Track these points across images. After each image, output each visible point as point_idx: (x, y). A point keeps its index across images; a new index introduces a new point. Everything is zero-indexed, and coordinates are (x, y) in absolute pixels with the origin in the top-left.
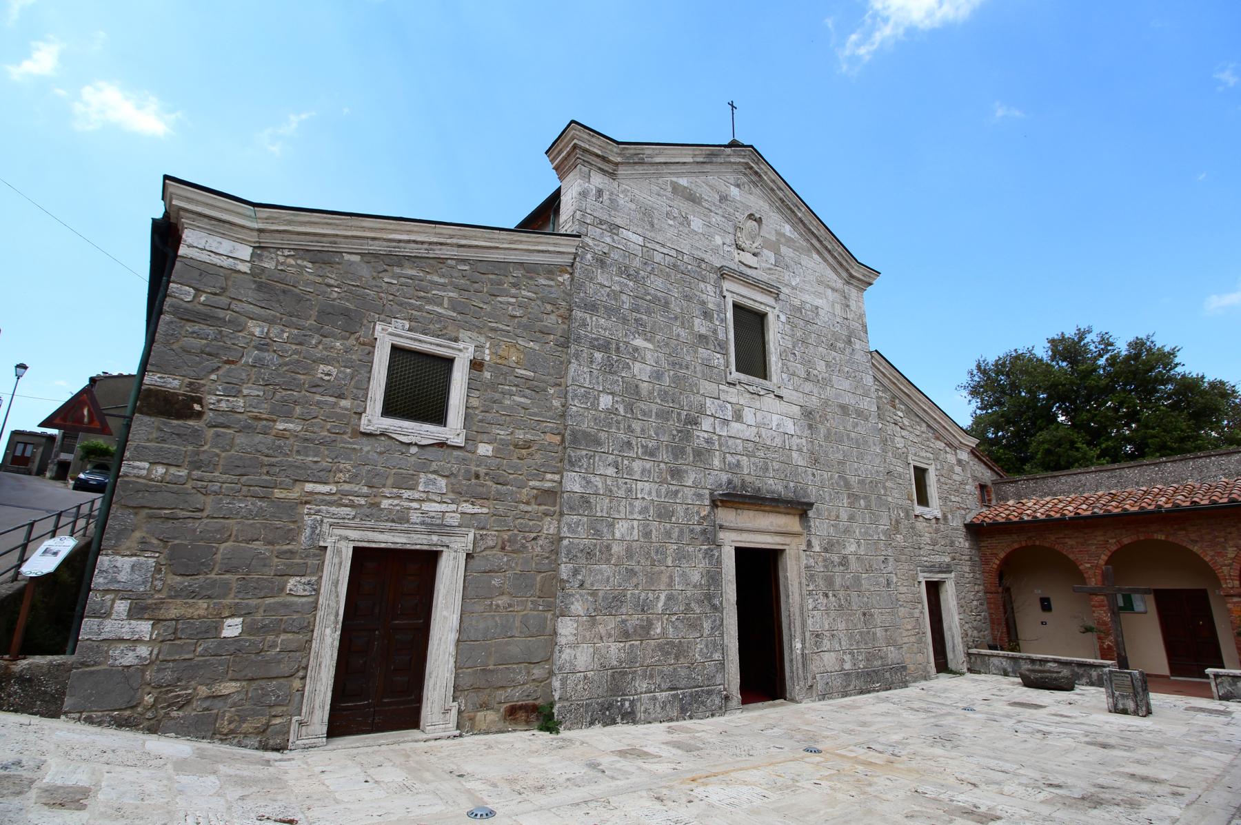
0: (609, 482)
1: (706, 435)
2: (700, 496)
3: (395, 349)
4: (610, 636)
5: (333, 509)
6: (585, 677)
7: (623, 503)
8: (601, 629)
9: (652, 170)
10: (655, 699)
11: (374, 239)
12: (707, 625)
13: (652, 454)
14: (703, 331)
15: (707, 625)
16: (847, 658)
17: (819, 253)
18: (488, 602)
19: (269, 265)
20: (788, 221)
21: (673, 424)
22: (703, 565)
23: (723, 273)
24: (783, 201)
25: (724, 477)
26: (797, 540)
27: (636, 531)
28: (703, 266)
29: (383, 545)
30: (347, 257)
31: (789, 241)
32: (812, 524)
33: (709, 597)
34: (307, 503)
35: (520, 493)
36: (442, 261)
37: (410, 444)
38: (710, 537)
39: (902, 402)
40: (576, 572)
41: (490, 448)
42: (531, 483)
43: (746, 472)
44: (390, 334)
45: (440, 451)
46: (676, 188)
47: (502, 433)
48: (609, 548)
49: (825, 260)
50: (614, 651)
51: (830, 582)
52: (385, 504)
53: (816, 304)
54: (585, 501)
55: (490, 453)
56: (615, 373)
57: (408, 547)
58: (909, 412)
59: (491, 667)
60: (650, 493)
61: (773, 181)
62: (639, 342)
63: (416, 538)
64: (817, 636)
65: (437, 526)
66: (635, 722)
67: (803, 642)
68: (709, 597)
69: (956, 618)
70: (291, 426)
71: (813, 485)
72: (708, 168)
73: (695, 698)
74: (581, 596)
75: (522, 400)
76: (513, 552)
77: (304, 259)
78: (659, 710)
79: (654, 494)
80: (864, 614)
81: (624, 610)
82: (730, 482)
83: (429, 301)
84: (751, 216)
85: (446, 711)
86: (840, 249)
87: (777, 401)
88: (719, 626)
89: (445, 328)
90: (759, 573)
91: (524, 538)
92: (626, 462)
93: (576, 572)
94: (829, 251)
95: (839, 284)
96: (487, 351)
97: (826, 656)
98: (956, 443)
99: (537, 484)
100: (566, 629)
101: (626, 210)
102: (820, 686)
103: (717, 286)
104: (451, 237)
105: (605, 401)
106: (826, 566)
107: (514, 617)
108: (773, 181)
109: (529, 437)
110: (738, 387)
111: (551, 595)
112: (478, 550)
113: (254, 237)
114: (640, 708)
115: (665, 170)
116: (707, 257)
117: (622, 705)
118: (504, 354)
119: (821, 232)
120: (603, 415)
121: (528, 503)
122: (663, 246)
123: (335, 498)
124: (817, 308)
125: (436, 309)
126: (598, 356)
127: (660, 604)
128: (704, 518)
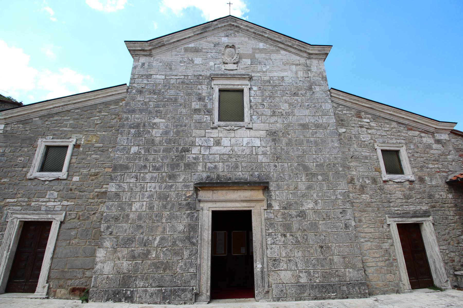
0: (131, 185)
1: (194, 156)
2: (187, 186)
4: (124, 258)
5: (14, 208)
6: (108, 277)
7: (138, 194)
8: (120, 255)
9: (172, 46)
10: (146, 291)
11: (41, 110)
12: (186, 254)
13: (158, 169)
14: (197, 107)
15: (186, 254)
16: (303, 275)
17: (284, 49)
18: (68, 242)
19: (9, 129)
20: (261, 41)
21: (173, 154)
22: (186, 221)
23: (212, 78)
24: (255, 33)
25: (205, 175)
26: (260, 204)
27: (144, 207)
28: (201, 78)
29: (30, 220)
30: (34, 119)
31: (261, 51)
32: (273, 193)
33: (189, 238)
34: (6, 206)
35: (89, 195)
36: (69, 111)
37: (45, 181)
38: (192, 207)
39: (366, 113)
40: (108, 228)
41: (78, 178)
42: (95, 190)
43: (220, 170)
44: (45, 142)
45: (56, 182)
46: (186, 50)
47: (85, 171)
48: (128, 216)
49: (290, 52)
50: (125, 265)
51: (288, 227)
52: (33, 204)
53: (282, 75)
54: (117, 195)
55: (78, 180)
56: (141, 136)
57: (39, 220)
58: (375, 118)
59: (66, 270)
60: (155, 188)
61: (247, 26)
62: (157, 120)
63: (42, 216)
65: (49, 211)
66: (132, 302)
67: (263, 264)
68: (189, 238)
69: (437, 249)
70: (6, 180)
71: (273, 173)
72: (206, 34)
73: (173, 292)
74: (110, 238)
75: (96, 156)
76: (83, 220)
77: (19, 124)
78: (148, 297)
79: (157, 188)
80: (322, 247)
81: (133, 245)
82: (208, 177)
83: (63, 127)
84: (227, 46)
85: (44, 287)
86: (297, 43)
87: (248, 131)
88: (195, 254)
89: (66, 135)
91: (89, 214)
92: (142, 175)
93: (108, 228)
94: (291, 46)
95: (303, 61)
96: (83, 140)
97: (282, 274)
98: (432, 130)
99: (98, 190)
100: (101, 254)
101: (157, 67)
102: (275, 292)
103: (209, 84)
104: (69, 101)
105: (134, 149)
107: (79, 248)
108: (247, 26)
109: (97, 171)
110: (219, 129)
111: (97, 239)
112: (67, 220)
114: (136, 295)
115: (179, 43)
116: (202, 74)
117: (126, 293)
118: (90, 139)
119: (283, 39)
120: (132, 156)
121: (93, 199)
122: (176, 76)
123: (15, 203)
124: (283, 77)
125: (65, 129)
126: (133, 131)
127: (156, 242)
128: (189, 197)
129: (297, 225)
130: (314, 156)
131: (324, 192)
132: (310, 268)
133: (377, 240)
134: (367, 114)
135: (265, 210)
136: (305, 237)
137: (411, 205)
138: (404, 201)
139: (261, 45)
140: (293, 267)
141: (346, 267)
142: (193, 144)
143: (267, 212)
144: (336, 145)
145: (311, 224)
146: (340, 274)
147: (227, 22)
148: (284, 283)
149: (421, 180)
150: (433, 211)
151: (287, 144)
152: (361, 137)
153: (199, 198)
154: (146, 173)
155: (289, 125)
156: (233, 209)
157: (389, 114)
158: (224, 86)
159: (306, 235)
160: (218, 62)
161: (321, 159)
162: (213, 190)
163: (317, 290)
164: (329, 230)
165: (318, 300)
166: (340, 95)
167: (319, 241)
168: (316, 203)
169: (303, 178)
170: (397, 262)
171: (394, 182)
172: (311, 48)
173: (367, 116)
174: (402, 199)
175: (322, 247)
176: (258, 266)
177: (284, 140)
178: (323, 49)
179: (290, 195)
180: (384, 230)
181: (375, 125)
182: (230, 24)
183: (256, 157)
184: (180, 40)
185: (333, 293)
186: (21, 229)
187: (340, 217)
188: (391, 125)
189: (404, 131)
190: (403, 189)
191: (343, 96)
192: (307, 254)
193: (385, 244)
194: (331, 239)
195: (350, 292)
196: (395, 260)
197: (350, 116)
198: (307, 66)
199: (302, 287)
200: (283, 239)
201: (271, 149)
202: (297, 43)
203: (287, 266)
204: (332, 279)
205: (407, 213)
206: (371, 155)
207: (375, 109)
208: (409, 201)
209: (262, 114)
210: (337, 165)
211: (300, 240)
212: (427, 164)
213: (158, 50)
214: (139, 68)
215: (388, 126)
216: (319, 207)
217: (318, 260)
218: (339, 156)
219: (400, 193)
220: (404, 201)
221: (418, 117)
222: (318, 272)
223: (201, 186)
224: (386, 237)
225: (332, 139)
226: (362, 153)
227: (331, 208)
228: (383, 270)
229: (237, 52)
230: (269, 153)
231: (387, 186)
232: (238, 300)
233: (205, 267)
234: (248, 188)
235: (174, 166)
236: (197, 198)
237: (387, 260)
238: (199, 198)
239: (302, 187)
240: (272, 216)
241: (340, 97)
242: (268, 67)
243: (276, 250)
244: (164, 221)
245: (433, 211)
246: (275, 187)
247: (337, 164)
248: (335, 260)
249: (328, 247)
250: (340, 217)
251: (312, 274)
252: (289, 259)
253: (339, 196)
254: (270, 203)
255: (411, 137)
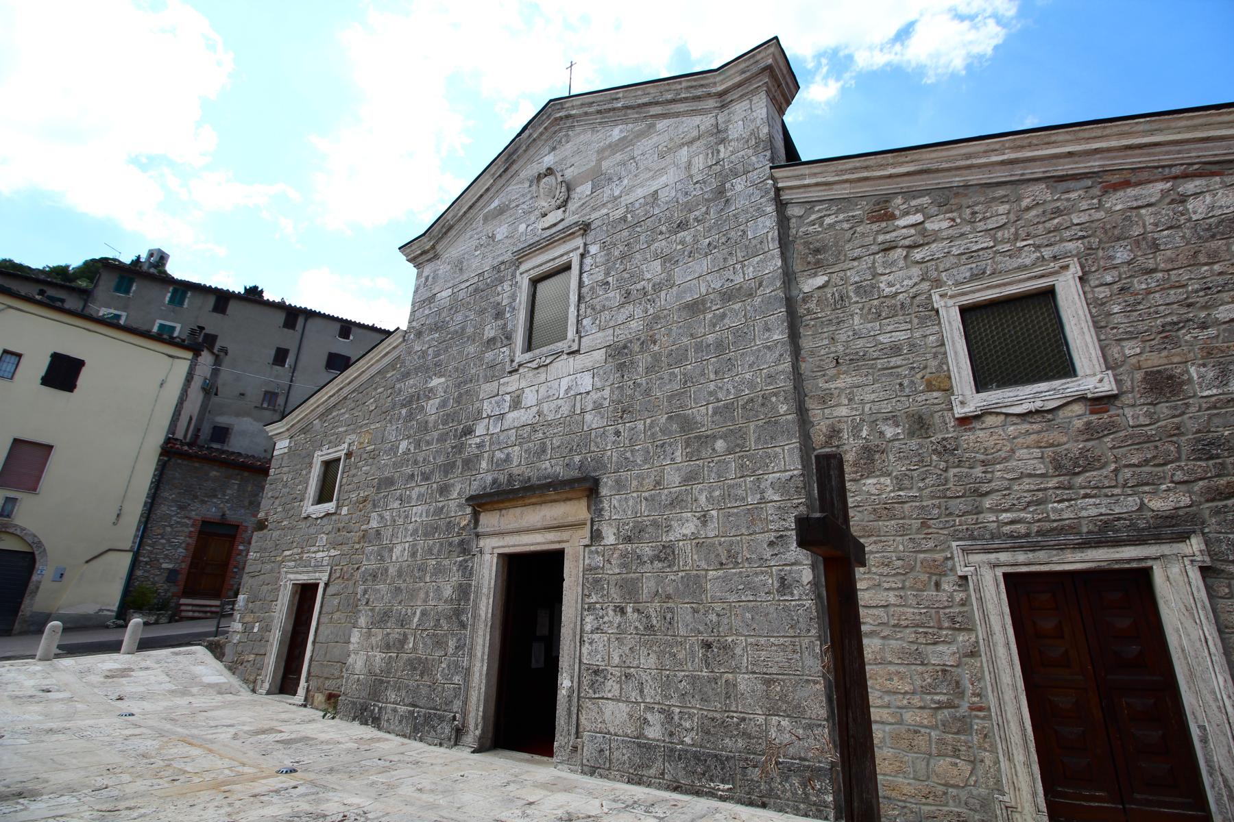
3: (965, 311)
10: (395, 710)
12: (452, 643)
15: (452, 643)
17: (664, 116)
20: (615, 123)
22: (456, 578)
31: (614, 148)
32: (606, 505)
33: (458, 613)
39: (910, 194)
48: (387, 570)
49: (677, 115)
51: (630, 589)
58: (946, 199)
64: (596, 672)
66: (379, 728)
68: (458, 613)
72: (515, 167)
73: (428, 719)
80: (708, 646)
82: (495, 481)
90: (533, 584)
93: (365, 592)
102: (588, 751)
106: (624, 565)
113: (287, 434)
127: (416, 620)
129: (652, 584)
130: (712, 386)
131: (730, 486)
132: (673, 702)
133: (909, 634)
134: (914, 198)
135: (586, 546)
136: (669, 616)
137: (1086, 496)
138: (1052, 483)
139: (616, 133)
140: (634, 694)
141: (772, 711)
142: (478, 416)
143: (591, 552)
144: (776, 337)
145: (687, 580)
146: (753, 730)
147: (548, 117)
148: (609, 733)
149: (1162, 385)
150: (1217, 512)
151: (649, 370)
152: (882, 285)
153: (480, 530)
154: (413, 488)
155: (657, 318)
156: (532, 548)
157: (1003, 163)
158: (551, 263)
159: (670, 610)
160: (533, 219)
161: (727, 390)
162: (500, 510)
163: (681, 765)
164: (733, 598)
165: (681, 793)
166: (802, 177)
167: (701, 629)
168: (704, 519)
169: (678, 453)
170: (989, 717)
171: (1007, 415)
172: (718, 79)
173: (913, 203)
174: (1042, 475)
175: (708, 646)
176: (565, 683)
177: (643, 360)
178: (752, 61)
179: (644, 503)
180: (943, 597)
181: (946, 224)
182: (556, 119)
183: (580, 418)
184: (474, 204)
185: (723, 782)
186: (297, 597)
187: (768, 556)
188: (1019, 199)
189: (1084, 205)
190: (1054, 436)
191: (815, 174)
192: (668, 663)
193: (940, 648)
194: (736, 622)
195: (771, 790)
196: (980, 709)
197: (846, 226)
198: (719, 132)
199: (645, 748)
200: (618, 619)
201: (612, 392)
202: (684, 85)
203: (621, 689)
204: (727, 740)
205: (1061, 531)
206: (917, 335)
207: (937, 171)
208: (1079, 480)
209: (604, 308)
210: (774, 399)
211: (655, 622)
212: (1205, 307)
213: (445, 241)
214: (422, 290)
215: (1003, 208)
216: (711, 530)
217: (694, 680)
218: (780, 368)
219: (1037, 452)
220: (1052, 483)
221: (1142, 125)
222: (691, 716)
223: (481, 503)
224: (946, 625)
225: (766, 323)
226: (881, 338)
227: (744, 531)
228: (920, 742)
229: (560, 179)
230: (606, 403)
231: (978, 436)
232: (537, 757)
233: (477, 675)
234: (556, 497)
235: (448, 468)
236: (475, 528)
237: (941, 706)
238: (480, 530)
239: (673, 478)
240: (599, 560)
241: (806, 182)
242: (625, 182)
243: (600, 648)
244: (428, 579)
245: (1217, 512)
246: (611, 488)
247: (775, 395)
248: (742, 687)
249: (725, 647)
250: (768, 556)
251: (676, 718)
252: (628, 671)
253: (771, 495)
254: (598, 530)
255: (1118, 218)
